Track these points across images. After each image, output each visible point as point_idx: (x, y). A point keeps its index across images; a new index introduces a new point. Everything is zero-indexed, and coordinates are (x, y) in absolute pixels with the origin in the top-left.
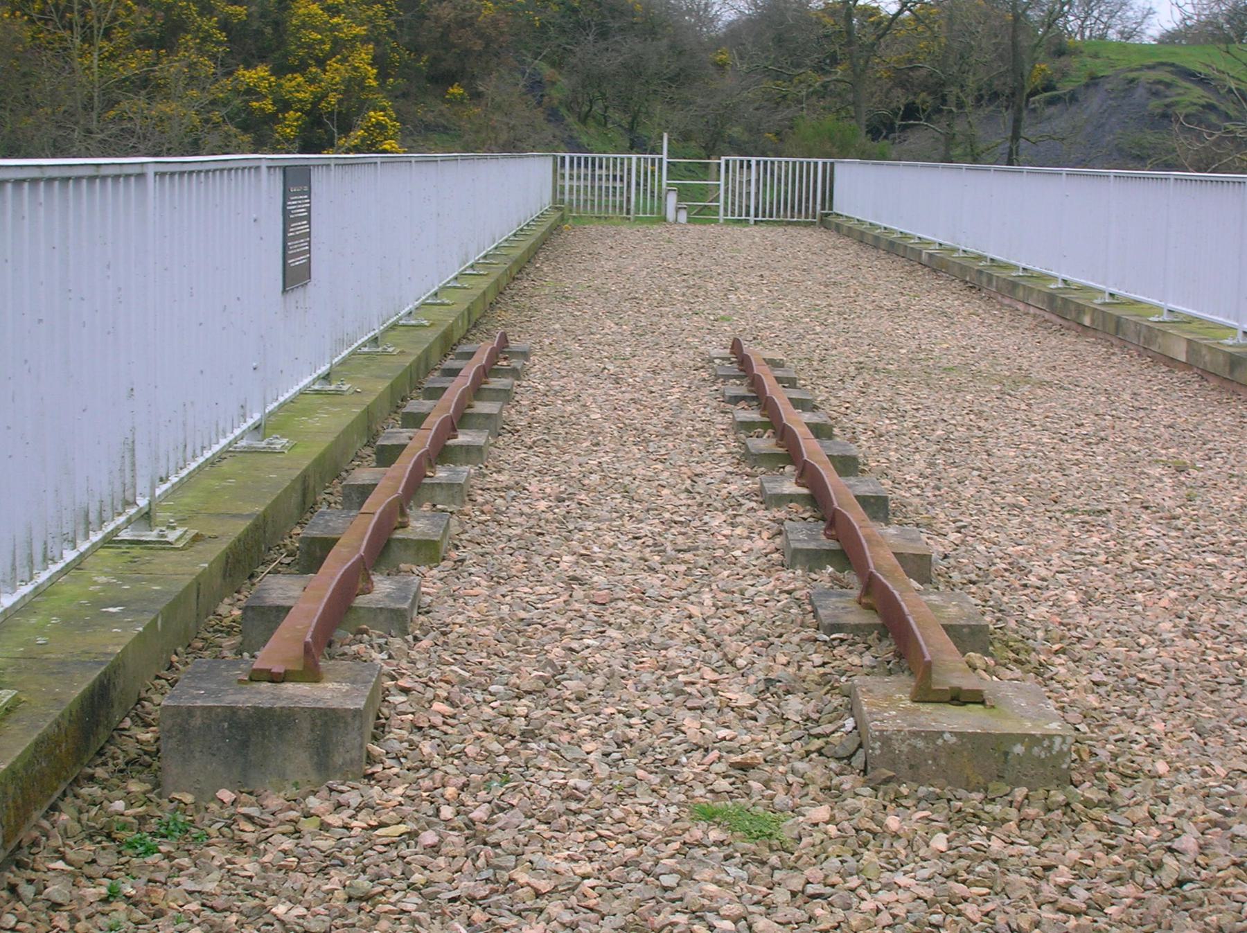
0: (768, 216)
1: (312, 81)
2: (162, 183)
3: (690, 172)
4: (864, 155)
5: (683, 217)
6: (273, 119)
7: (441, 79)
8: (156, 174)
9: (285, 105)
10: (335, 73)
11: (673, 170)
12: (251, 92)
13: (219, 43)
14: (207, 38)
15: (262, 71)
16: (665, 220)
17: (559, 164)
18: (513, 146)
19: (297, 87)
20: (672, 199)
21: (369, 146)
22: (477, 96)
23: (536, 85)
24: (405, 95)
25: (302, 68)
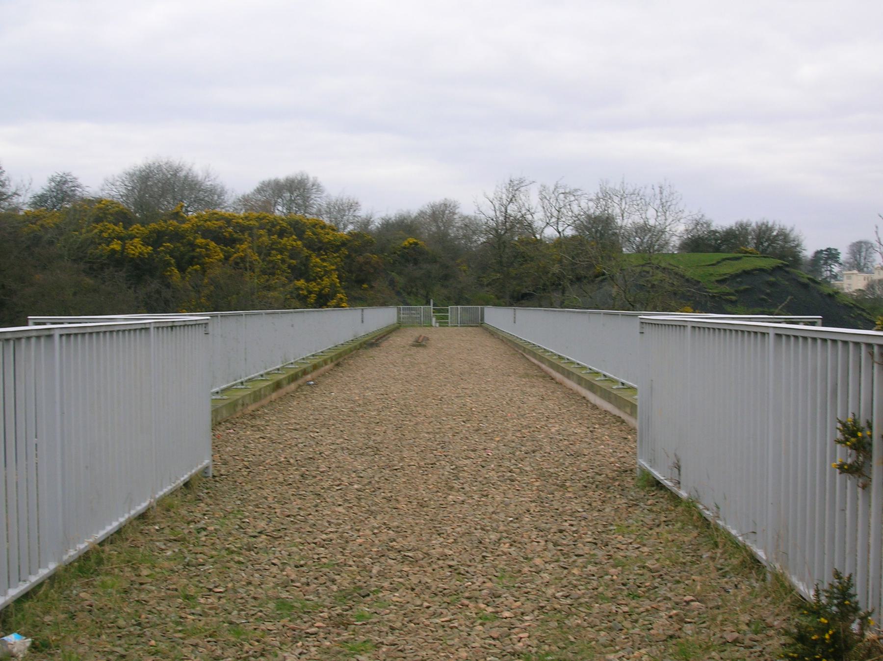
0: (464, 324)
1: (318, 284)
2: (158, 332)
3: (439, 311)
4: (495, 305)
5: (437, 325)
6: (306, 297)
7: (360, 282)
8: (61, 336)
9: (310, 292)
10: (326, 281)
11: (436, 311)
12: (299, 289)
13: (288, 273)
14: (284, 271)
15: (302, 281)
16: (432, 326)
17: (399, 310)
18: (384, 304)
19: (314, 287)
20: (434, 320)
21: (338, 306)
22: (372, 287)
23: (392, 283)
24: (348, 288)
25: (315, 280)
